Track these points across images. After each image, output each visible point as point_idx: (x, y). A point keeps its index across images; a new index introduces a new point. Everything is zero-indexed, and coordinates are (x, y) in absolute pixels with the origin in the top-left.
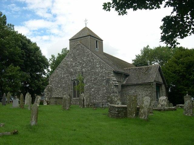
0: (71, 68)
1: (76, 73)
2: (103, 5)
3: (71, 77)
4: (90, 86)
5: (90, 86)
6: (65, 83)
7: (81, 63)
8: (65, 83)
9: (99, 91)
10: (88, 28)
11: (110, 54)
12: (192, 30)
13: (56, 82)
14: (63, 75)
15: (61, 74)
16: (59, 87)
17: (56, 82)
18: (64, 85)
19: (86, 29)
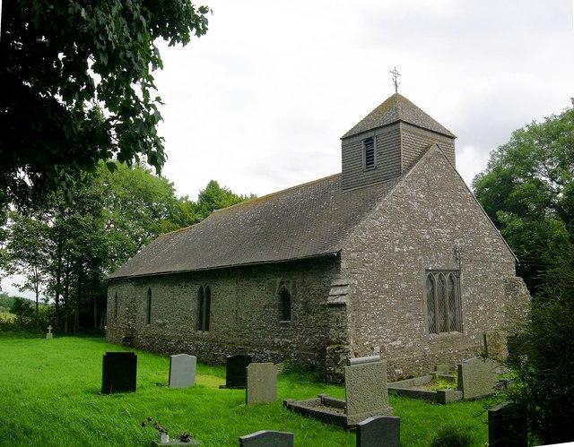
0: (422, 227)
1: (437, 248)
2: (173, 184)
3: (425, 259)
4: (474, 296)
5: (474, 296)
6: (409, 279)
7: (448, 220)
8: (409, 279)
9: (493, 312)
10: (406, 102)
11: (271, 193)
12: (20, 170)
13: (372, 268)
14: (399, 246)
15: (391, 238)
16: (386, 292)
17: (372, 268)
18: (404, 285)
19: (395, 102)
